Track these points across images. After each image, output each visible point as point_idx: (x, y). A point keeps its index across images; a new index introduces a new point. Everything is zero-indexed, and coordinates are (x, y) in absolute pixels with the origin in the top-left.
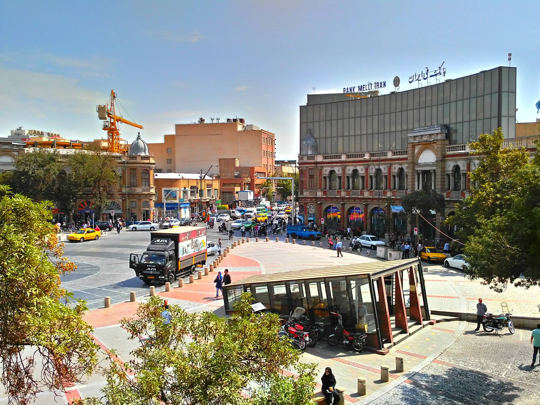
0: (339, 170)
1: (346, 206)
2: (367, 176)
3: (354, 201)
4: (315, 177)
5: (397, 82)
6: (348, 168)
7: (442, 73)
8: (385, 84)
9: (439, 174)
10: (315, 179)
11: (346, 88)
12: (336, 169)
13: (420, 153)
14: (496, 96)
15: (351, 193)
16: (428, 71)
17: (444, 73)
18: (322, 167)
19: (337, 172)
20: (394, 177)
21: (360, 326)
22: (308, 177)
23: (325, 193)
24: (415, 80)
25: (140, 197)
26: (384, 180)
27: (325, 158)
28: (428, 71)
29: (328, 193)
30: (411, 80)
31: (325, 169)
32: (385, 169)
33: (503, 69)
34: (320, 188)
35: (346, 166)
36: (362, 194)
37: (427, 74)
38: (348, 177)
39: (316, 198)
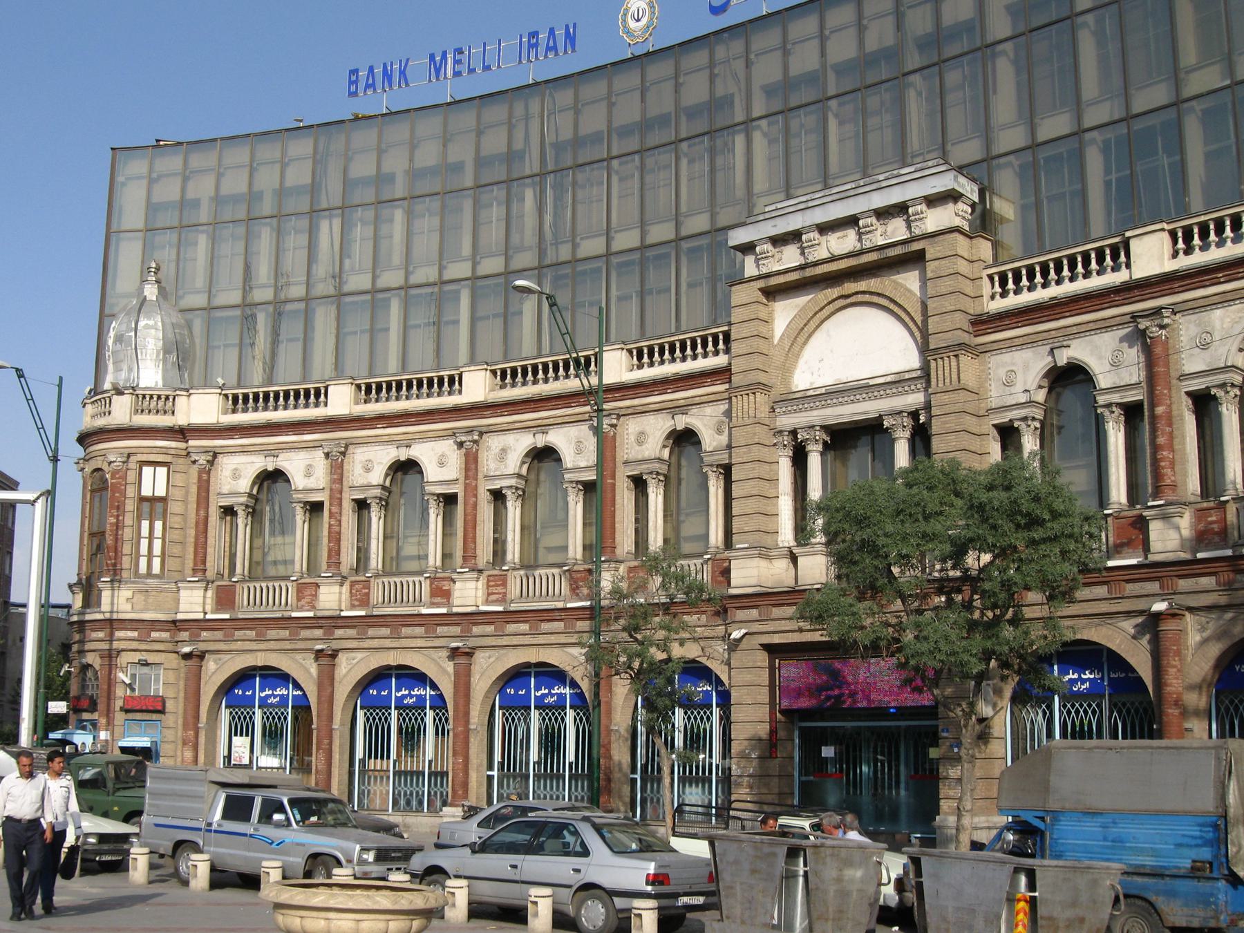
0: (309, 472)
1: (343, 662)
2: (471, 490)
4: (174, 507)
6: (359, 455)
8: (570, 38)
10: (174, 521)
12: (424, 453)
13: (802, 333)
15: (376, 595)
19: (299, 480)
20: (639, 483)
21: (1017, 837)
22: (130, 506)
23: (225, 598)
26: (576, 507)
27: (237, 402)
29: (242, 596)
31: (227, 464)
34: (200, 567)
36: (441, 593)
38: (362, 505)
39: (175, 625)
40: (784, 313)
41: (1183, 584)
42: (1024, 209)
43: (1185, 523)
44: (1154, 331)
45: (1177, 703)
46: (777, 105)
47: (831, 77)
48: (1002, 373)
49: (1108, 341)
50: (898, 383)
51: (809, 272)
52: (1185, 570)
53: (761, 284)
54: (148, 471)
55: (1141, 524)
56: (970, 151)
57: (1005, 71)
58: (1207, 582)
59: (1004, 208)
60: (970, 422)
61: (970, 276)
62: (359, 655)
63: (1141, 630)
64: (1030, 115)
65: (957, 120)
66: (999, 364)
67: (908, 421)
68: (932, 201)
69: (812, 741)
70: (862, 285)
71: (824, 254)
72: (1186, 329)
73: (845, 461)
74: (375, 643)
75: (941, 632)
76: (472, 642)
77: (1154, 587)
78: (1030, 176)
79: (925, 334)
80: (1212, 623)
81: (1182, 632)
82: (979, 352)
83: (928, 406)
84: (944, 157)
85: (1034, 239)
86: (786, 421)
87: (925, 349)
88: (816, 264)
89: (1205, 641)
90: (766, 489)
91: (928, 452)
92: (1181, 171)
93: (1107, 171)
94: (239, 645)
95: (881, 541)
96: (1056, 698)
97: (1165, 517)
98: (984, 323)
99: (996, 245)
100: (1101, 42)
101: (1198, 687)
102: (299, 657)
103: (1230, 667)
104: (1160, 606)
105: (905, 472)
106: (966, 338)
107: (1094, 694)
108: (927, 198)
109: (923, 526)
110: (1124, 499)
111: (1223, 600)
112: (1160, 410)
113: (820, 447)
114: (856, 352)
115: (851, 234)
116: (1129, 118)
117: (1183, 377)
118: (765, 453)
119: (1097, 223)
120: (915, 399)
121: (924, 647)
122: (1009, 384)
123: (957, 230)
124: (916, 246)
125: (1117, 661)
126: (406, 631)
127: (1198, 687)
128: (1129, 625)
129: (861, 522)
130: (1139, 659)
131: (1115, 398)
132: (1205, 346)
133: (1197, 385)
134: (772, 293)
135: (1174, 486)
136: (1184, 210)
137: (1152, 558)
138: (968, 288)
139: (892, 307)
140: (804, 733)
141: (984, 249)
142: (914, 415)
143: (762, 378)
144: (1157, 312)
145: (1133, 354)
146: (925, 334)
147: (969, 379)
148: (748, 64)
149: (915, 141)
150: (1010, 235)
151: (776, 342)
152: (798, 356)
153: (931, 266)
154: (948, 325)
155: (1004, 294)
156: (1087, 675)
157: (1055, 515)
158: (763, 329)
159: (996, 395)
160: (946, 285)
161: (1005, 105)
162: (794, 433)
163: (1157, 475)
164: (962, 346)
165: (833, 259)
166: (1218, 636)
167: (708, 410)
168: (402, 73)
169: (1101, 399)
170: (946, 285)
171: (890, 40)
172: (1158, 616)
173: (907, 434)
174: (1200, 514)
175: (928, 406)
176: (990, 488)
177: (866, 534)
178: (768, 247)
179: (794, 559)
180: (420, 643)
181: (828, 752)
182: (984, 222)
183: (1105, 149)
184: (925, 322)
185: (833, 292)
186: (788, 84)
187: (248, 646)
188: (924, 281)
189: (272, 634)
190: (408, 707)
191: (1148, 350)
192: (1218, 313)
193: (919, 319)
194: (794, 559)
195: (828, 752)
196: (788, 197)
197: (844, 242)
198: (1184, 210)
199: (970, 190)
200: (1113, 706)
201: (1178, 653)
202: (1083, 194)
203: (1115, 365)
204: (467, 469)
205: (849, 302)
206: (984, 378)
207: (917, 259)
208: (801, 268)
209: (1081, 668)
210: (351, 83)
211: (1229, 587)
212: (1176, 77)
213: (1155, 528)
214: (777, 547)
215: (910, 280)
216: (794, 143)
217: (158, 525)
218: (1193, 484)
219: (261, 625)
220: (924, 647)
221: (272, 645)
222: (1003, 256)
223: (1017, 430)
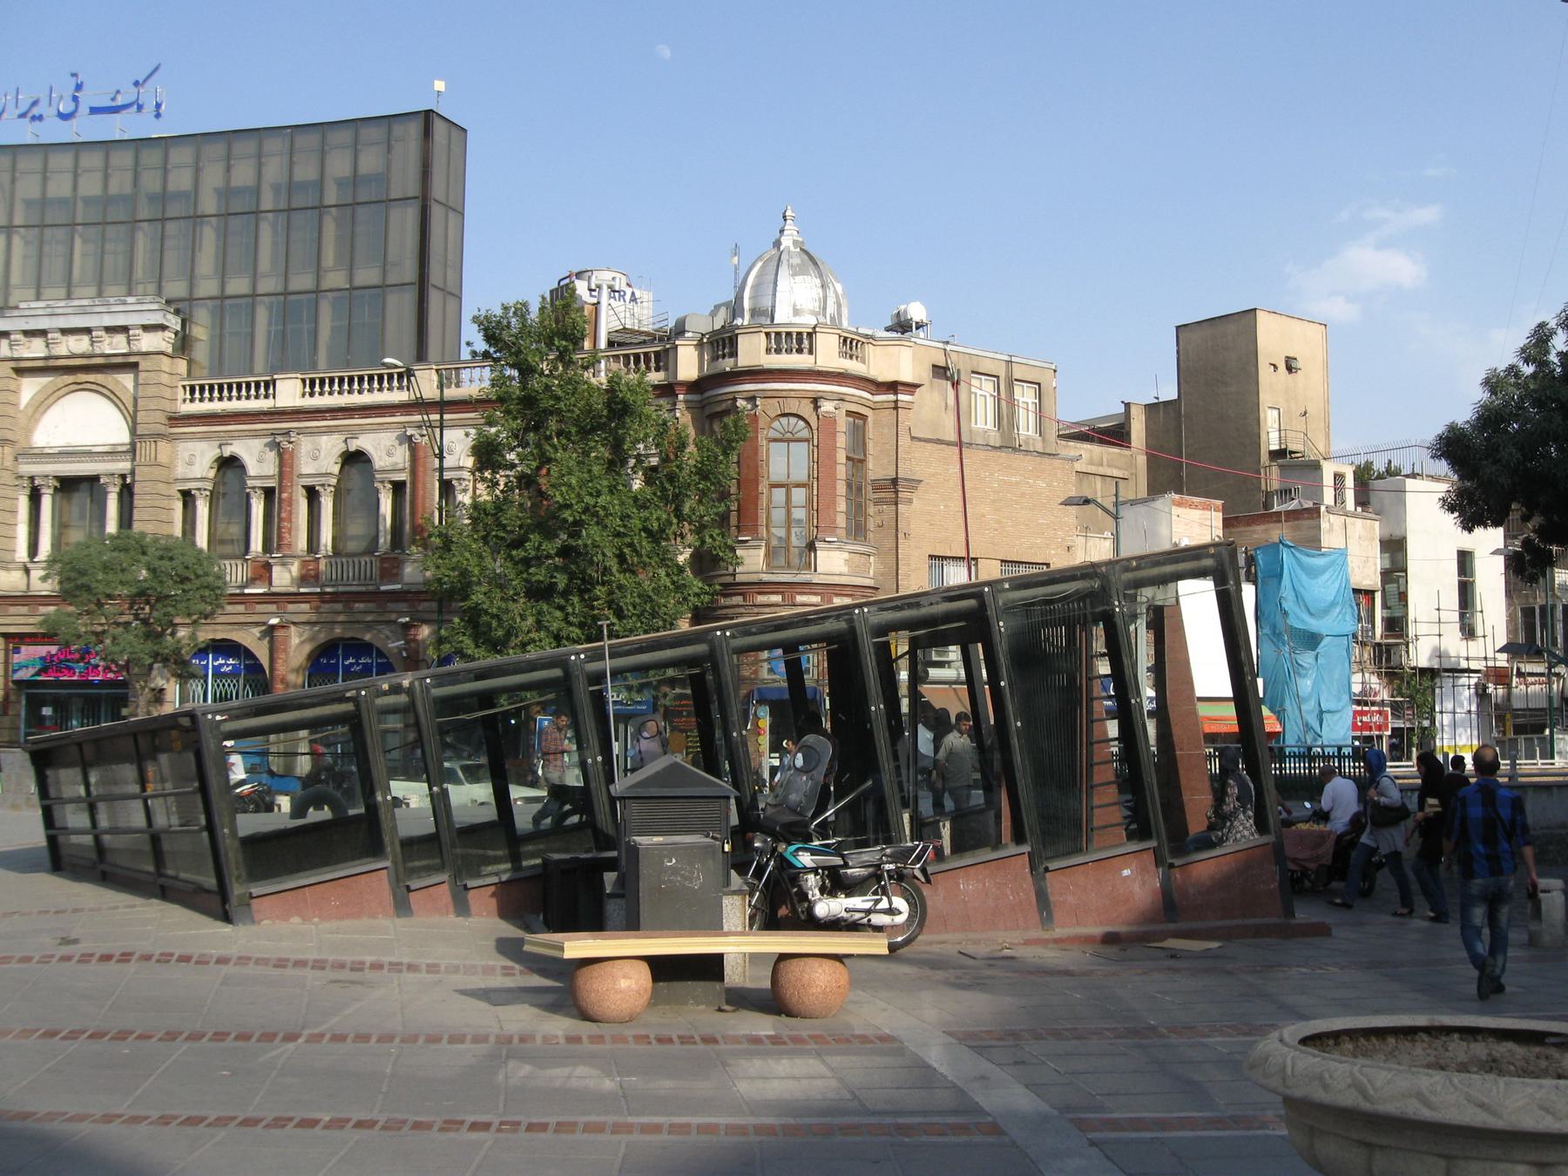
7: (150, 107)
13: (43, 404)
16: (79, 87)
28: (79, 87)
37: (75, 99)
40: (30, 388)
41: (291, 607)
42: (212, 337)
43: (295, 568)
44: (285, 445)
45: (283, 681)
46: (34, 220)
47: (80, 205)
48: (186, 455)
49: (258, 444)
50: (112, 453)
51: (52, 363)
52: (292, 598)
53: (13, 364)
55: (268, 567)
56: (177, 289)
57: (209, 237)
58: (305, 607)
59: (200, 332)
60: (162, 488)
61: (170, 384)
63: (264, 634)
64: (223, 276)
65: (172, 261)
66: (186, 449)
67: (118, 481)
68: (147, 328)
69: (35, 703)
70: (91, 377)
71: (64, 352)
72: (305, 445)
73: (69, 500)
75: (130, 644)
77: (273, 608)
78: (219, 316)
79: (134, 419)
80: (307, 632)
81: (289, 637)
83: (133, 473)
84: (159, 293)
85: (218, 368)
86: (27, 469)
87: (133, 431)
88: (57, 358)
89: (302, 643)
90: (7, 517)
91: (130, 526)
92: (315, 334)
93: (270, 324)
95: (94, 585)
97: (283, 564)
98: (177, 419)
99: (190, 362)
100: (275, 231)
101: (297, 671)
103: (317, 659)
104: (274, 621)
105: (112, 537)
106: (162, 429)
107: (234, 674)
108: (140, 322)
109: (121, 576)
110: (260, 549)
111: (314, 618)
112: (285, 495)
113: (51, 491)
114: (83, 425)
115: (86, 339)
116: (286, 293)
117: (300, 476)
118: (9, 492)
119: (260, 363)
120: (124, 466)
121: (116, 649)
122: (190, 464)
123: (162, 353)
124: (132, 359)
125: (249, 654)
127: (297, 671)
128: (256, 631)
129: (83, 573)
130: (262, 655)
131: (258, 483)
132: (315, 459)
133: (309, 482)
134: (20, 372)
135: (290, 545)
136: (314, 366)
137: (274, 590)
138: (168, 393)
139: (112, 396)
140: (30, 698)
141: (182, 366)
142: (123, 477)
143: (9, 435)
144: (287, 433)
145: (272, 456)
146: (134, 419)
147: (163, 458)
148: (13, 181)
149: (139, 273)
150: (201, 352)
151: (22, 407)
152: (37, 421)
153: (142, 375)
154: (150, 420)
155: (192, 400)
156: (231, 661)
157: (198, 577)
158: (12, 398)
159: (180, 470)
160: (151, 391)
161: (206, 261)
162: (32, 478)
163: (280, 538)
164: (161, 436)
165: (73, 356)
166: (311, 639)
169: (250, 483)
170: (151, 391)
171: (128, 190)
172: (273, 627)
173: (117, 489)
174: (304, 564)
175: (133, 473)
176: (161, 558)
177: (84, 580)
178: (20, 337)
179: (27, 571)
181: (47, 711)
182: (184, 344)
183: (270, 309)
184: (136, 411)
185: (69, 379)
186: (44, 203)
188: (137, 384)
190: (225, 675)
191: (280, 455)
192: (325, 438)
193: (131, 409)
194: (27, 571)
195: (47, 711)
196: (38, 299)
197: (80, 345)
198: (314, 366)
199: (174, 322)
200: (246, 681)
201: (285, 651)
202: (252, 335)
203: (260, 461)
205: (81, 387)
206: (173, 457)
207: (134, 366)
208: (45, 358)
209: (227, 657)
211: (317, 610)
212: (319, 273)
213: (276, 570)
214: (13, 562)
215: (126, 380)
216: (46, 249)
218: (302, 543)
220: (116, 649)
222: (196, 371)
223: (193, 496)
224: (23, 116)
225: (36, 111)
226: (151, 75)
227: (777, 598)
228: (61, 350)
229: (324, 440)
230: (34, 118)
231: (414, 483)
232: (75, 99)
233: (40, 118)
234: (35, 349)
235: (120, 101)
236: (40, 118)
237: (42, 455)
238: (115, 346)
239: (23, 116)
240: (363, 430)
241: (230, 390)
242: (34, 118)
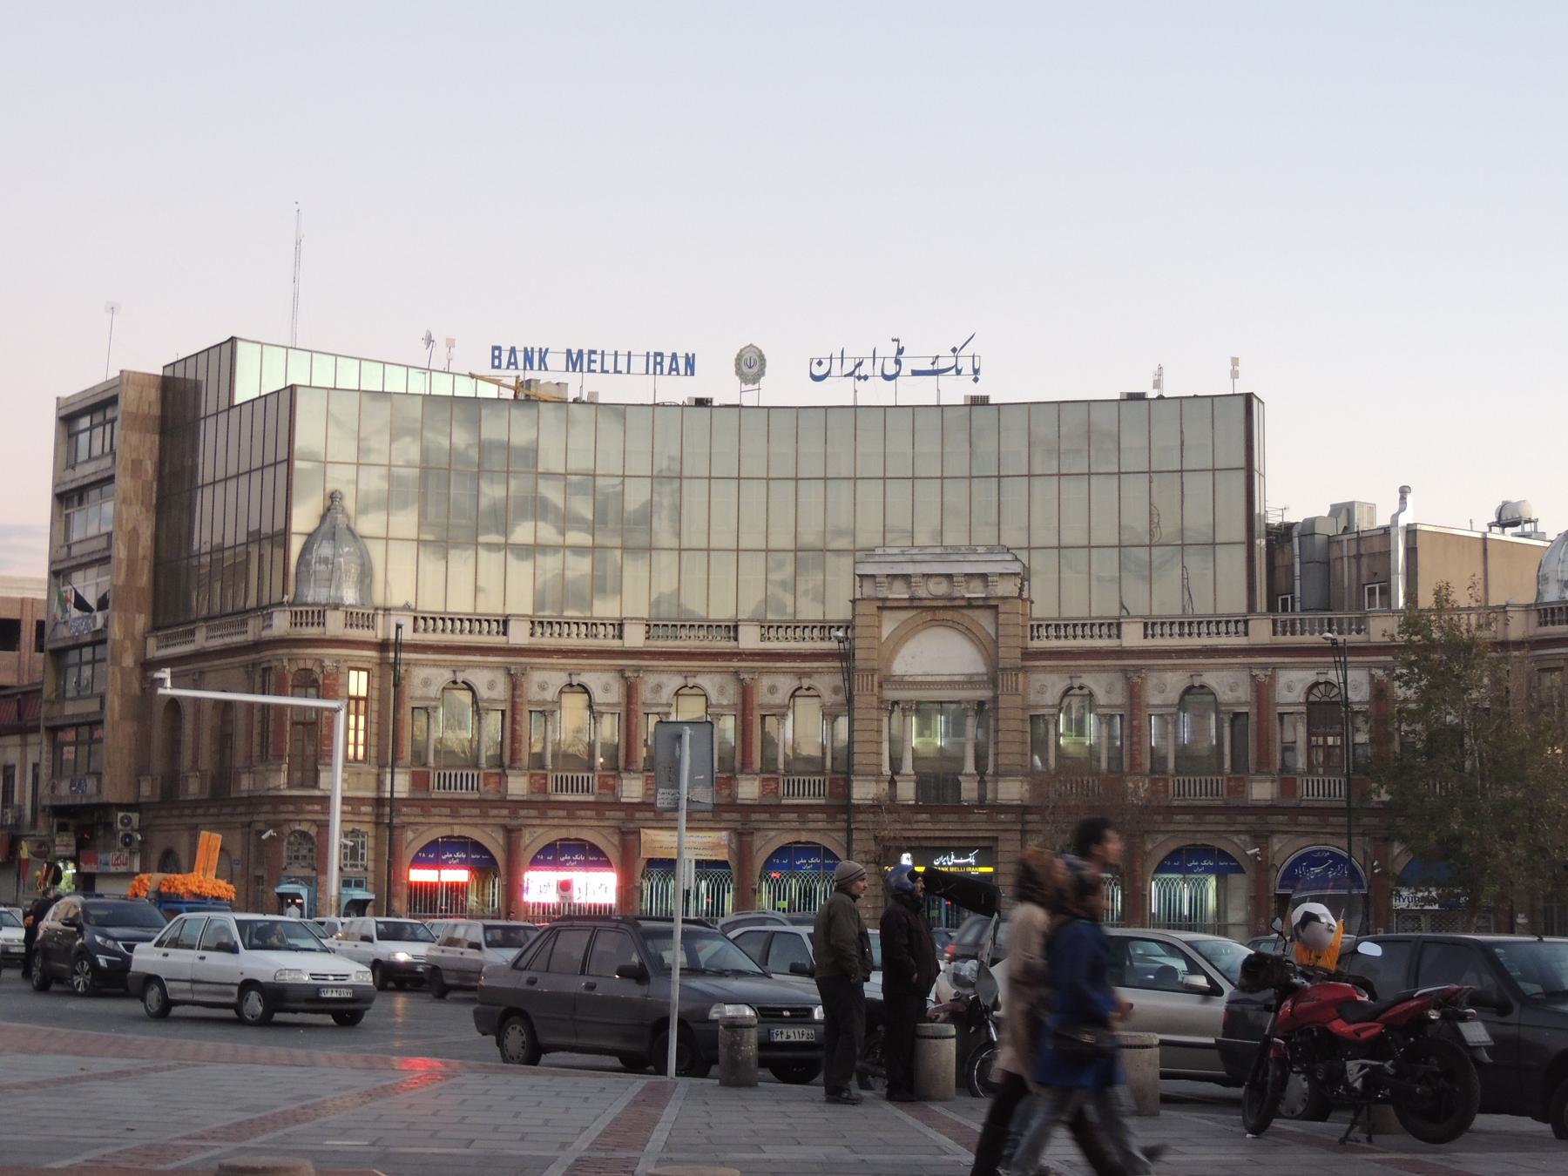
0: (491, 685)
1: (526, 837)
3: (571, 816)
5: (751, 366)
7: (967, 368)
8: (690, 363)
9: (1253, 719)
11: (506, 347)
13: (901, 638)
14: (282, 468)
16: (900, 351)
17: (976, 371)
18: (1275, 667)
24: (836, 370)
25: (631, 819)
28: (900, 351)
30: (818, 371)
32: (722, 691)
33: (299, 391)
35: (525, 670)
37: (898, 362)
48: (1038, 685)
49: (1104, 678)
51: (916, 603)
54: (353, 674)
62: (540, 831)
66: (1038, 679)
74: (556, 822)
76: (520, 822)
82: (1025, 669)
94: (437, 819)
96: (990, 870)
98: (1027, 655)
102: (488, 830)
106: (1019, 663)
112: (1135, 723)
120: (983, 694)
126: (551, 813)
139: (968, 632)
159: (1033, 698)
165: (936, 598)
167: (827, 678)
168: (542, 360)
180: (592, 823)
187: (444, 820)
189: (465, 811)
197: (941, 588)
204: (1255, 807)
210: (494, 357)
215: (984, 620)
217: (362, 719)
219: (455, 806)
221: (466, 820)
224: (851, 374)
225: (862, 371)
226: (295, 307)
227: (291, 808)
228: (922, 593)
229: (1169, 676)
230: (859, 378)
231: (1259, 714)
232: (898, 362)
233: (866, 378)
234: (899, 592)
235: (942, 365)
236: (866, 378)
237: (902, 683)
238: (976, 591)
239: (851, 374)
240: (1208, 668)
241: (1350, 624)
242: (859, 378)
